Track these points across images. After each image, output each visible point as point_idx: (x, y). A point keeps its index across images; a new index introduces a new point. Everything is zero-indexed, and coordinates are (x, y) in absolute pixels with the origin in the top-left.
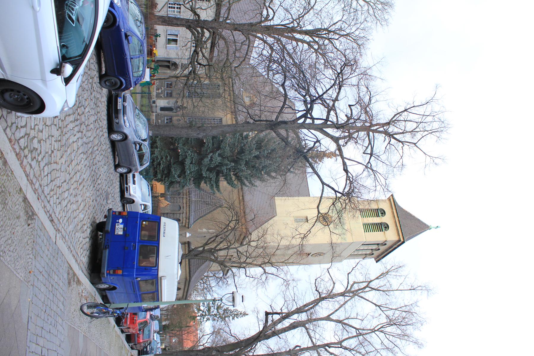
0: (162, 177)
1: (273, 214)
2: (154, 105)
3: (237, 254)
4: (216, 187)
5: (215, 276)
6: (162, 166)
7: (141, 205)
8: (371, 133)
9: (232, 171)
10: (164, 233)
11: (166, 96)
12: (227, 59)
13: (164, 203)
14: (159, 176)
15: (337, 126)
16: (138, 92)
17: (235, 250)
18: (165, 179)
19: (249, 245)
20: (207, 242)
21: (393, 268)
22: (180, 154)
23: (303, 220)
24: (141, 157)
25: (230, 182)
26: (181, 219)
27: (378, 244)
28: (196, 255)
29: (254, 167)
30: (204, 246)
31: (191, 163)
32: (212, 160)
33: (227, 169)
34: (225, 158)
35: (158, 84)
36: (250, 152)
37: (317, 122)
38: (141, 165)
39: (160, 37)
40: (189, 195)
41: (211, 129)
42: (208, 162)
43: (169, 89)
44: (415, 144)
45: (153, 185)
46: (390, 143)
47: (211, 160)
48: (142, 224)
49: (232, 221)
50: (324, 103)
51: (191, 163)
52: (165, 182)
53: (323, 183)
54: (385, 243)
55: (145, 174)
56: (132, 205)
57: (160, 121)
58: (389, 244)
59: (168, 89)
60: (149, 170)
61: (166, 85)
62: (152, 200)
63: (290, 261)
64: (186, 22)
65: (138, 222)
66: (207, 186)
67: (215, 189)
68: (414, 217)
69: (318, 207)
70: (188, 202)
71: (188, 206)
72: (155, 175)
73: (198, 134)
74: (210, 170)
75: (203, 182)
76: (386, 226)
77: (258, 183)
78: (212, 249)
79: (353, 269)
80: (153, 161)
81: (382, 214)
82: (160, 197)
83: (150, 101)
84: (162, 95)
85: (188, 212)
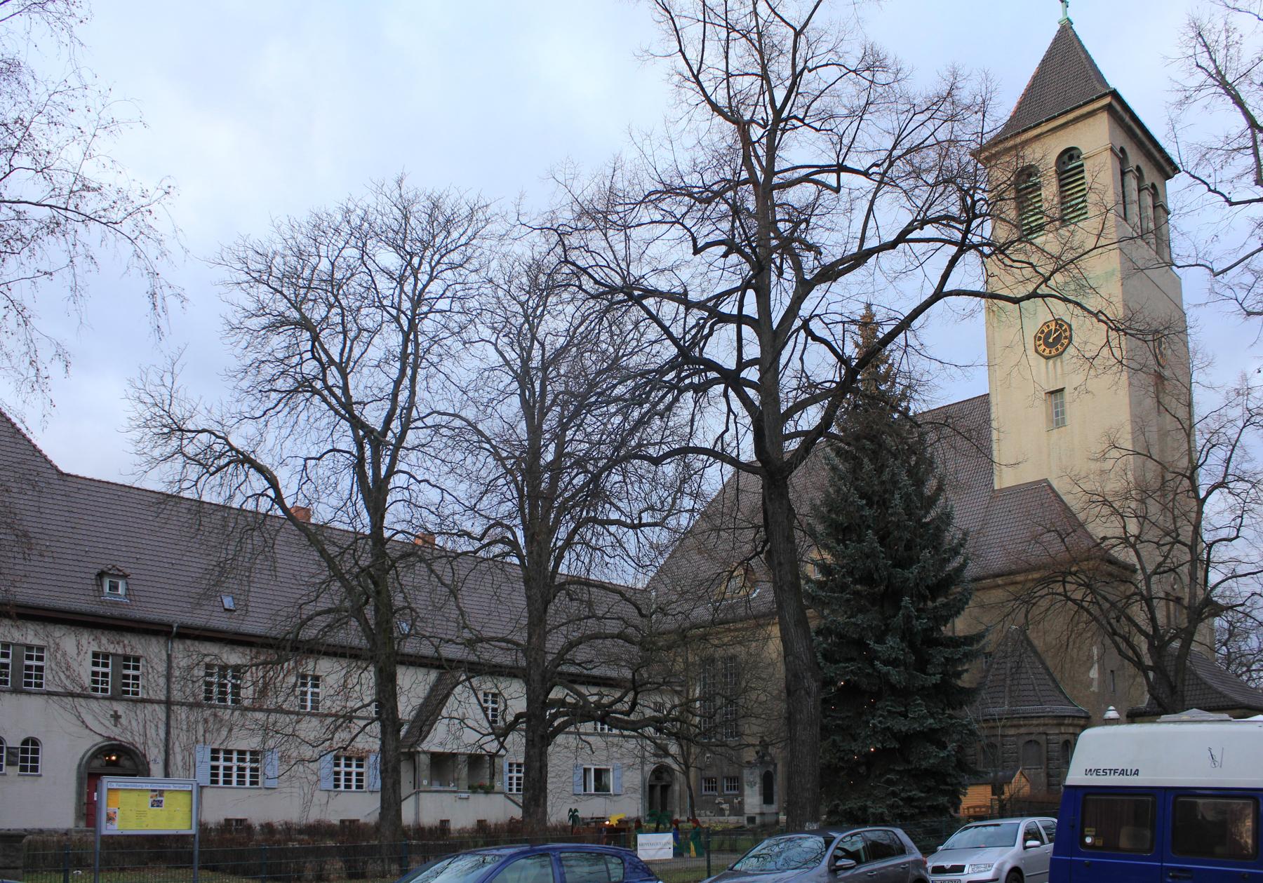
0: (944, 793)
1: (1043, 489)
2: (758, 820)
3: (1165, 572)
4: (971, 644)
5: (1228, 640)
6: (916, 793)
7: (1025, 848)
8: (776, 180)
9: (925, 604)
10: (1123, 772)
11: (736, 792)
12: (619, 636)
13: (1019, 784)
14: (943, 800)
15: (758, 282)
16: (705, 864)
17: (1154, 579)
18: (952, 785)
19: (1137, 537)
20: (1130, 659)
21: (1204, 60)
22: (879, 746)
23: (1056, 404)
24: (877, 851)
25: (956, 609)
26: (1062, 738)
27: (1123, 174)
28: (1173, 689)
29: (909, 547)
30: (1144, 669)
31: (906, 717)
32: (896, 659)
33: (918, 618)
34: (887, 625)
35: (708, 813)
36: (868, 557)
37: (753, 350)
38: (902, 851)
39: (576, 810)
40: (994, 720)
41: (791, 658)
42: (899, 672)
43: (719, 783)
44: (798, 34)
45: (970, 817)
46: (801, 117)
47: (894, 663)
48: (1092, 846)
49: (1066, 596)
50: (701, 337)
51: (906, 717)
52: (960, 783)
53: (939, 295)
54: (1118, 151)
55: (931, 839)
56: (1026, 874)
58: (1122, 141)
59: (719, 788)
60: (925, 826)
61: (711, 793)
62: (1012, 816)
63: (1182, 413)
64: (534, 746)
65: (1087, 860)
66: (966, 671)
67: (975, 647)
68: (1035, 78)
69: (1016, 301)
70: (1015, 722)
71: (1026, 722)
72: (941, 810)
73: (808, 693)
74: (922, 665)
75: (959, 683)
76: (1066, 157)
77: (952, 535)
78: (1151, 645)
79: (1215, 191)
80: (901, 819)
82: (1003, 797)
83: (748, 830)
84: (735, 801)
85: (1042, 721)
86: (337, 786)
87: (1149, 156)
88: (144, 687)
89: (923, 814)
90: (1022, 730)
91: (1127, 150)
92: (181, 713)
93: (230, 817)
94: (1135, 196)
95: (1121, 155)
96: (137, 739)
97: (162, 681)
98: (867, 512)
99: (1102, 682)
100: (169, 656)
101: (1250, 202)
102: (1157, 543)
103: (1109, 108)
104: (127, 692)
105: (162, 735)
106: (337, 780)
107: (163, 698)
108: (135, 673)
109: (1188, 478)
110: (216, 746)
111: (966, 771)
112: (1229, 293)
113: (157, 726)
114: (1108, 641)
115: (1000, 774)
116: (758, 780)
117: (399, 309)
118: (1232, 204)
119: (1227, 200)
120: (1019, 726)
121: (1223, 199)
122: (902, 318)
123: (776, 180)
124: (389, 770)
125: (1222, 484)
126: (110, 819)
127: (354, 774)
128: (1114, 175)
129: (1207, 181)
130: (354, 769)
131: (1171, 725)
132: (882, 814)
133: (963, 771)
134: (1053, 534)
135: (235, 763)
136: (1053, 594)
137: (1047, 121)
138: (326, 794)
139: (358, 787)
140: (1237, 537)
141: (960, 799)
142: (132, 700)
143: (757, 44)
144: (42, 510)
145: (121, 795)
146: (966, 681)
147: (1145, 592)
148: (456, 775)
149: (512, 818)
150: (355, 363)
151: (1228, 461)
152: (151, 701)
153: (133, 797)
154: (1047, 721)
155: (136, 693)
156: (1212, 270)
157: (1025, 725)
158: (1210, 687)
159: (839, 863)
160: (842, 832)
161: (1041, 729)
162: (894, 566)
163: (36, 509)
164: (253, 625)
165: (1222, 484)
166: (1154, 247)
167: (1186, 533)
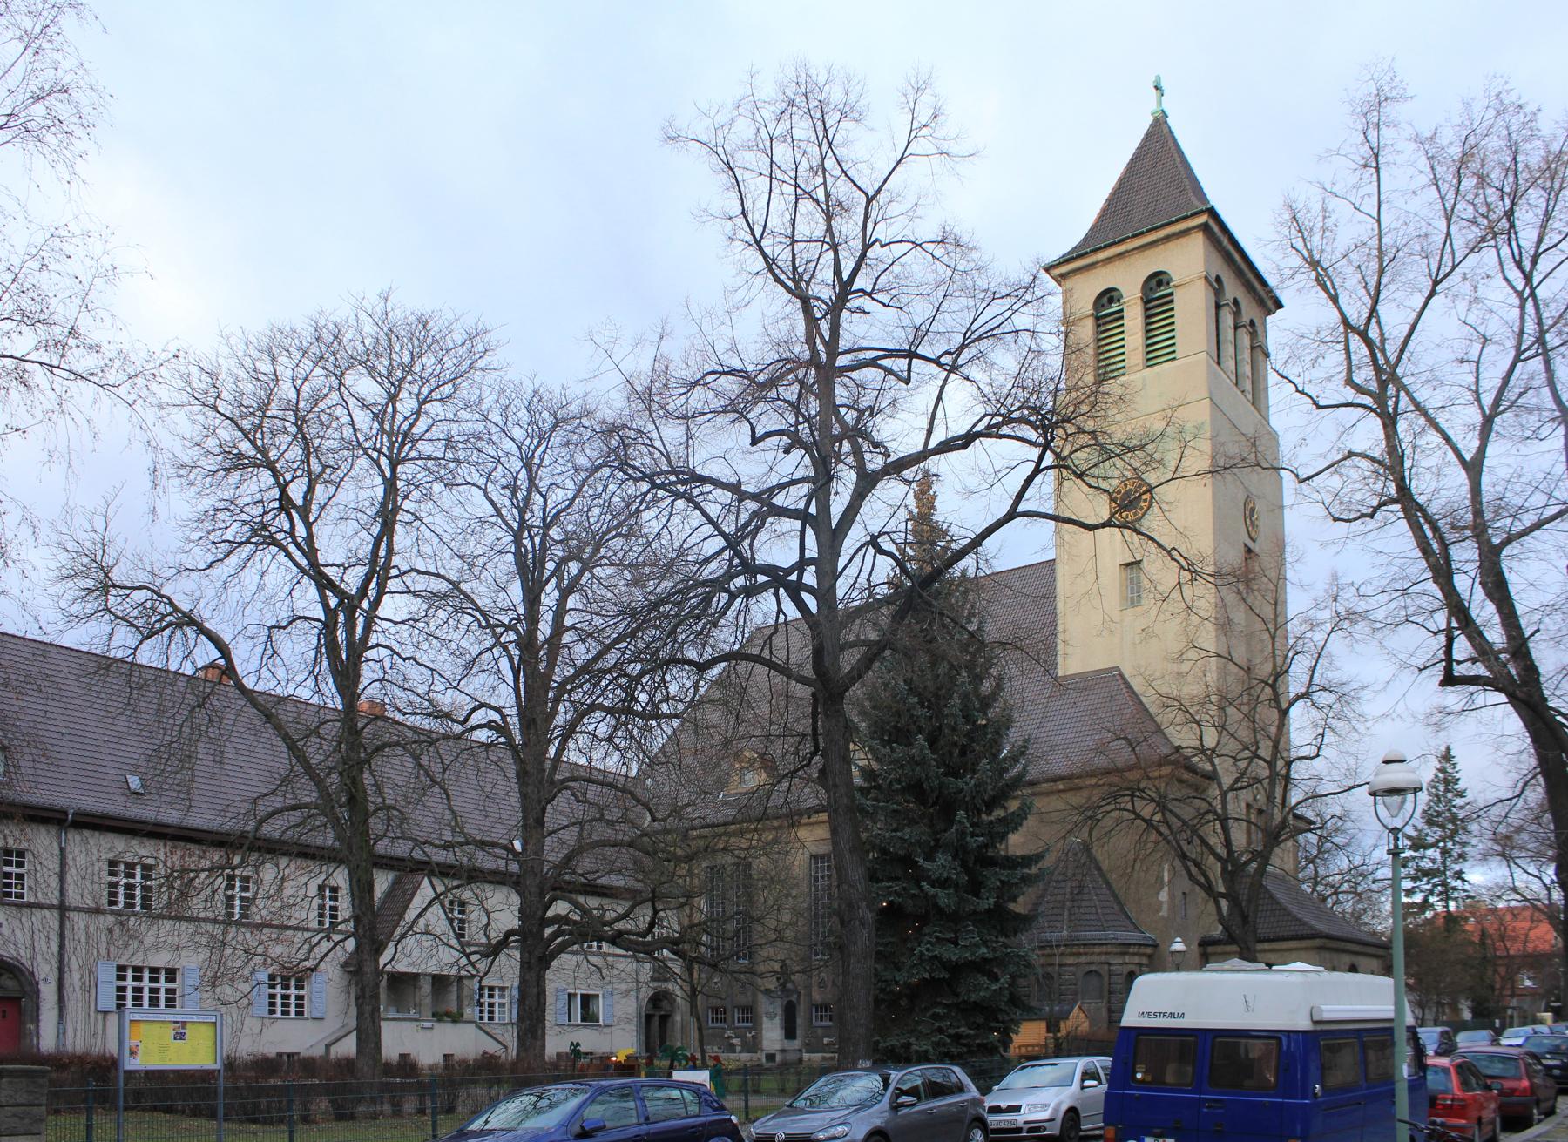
1: (1114, 677)
2: (778, 1058)
3: (1242, 788)
7: (1083, 1088)
10: (1171, 1015)
11: (750, 1025)
13: (1077, 1021)
15: (822, 482)
16: (742, 1104)
17: (1230, 795)
18: (1003, 1022)
19: (1213, 751)
20: (1200, 885)
21: (1299, 244)
25: (1013, 822)
26: (1126, 970)
27: (1218, 307)
28: (1245, 918)
31: (956, 944)
34: (937, 840)
35: (716, 1048)
37: (812, 551)
38: (961, 1089)
39: (578, 1044)
43: (729, 1014)
44: (870, 200)
47: (943, 883)
48: (1142, 1081)
49: (1134, 812)
50: (750, 530)
51: (956, 944)
53: (1011, 515)
55: (988, 1078)
56: (1082, 1115)
57: (826, 1040)
58: (1219, 268)
59: (729, 1019)
61: (718, 1025)
63: (1268, 612)
67: (1034, 870)
68: (1122, 181)
70: (1075, 950)
71: (1087, 950)
72: (990, 1050)
73: (863, 924)
74: (975, 887)
78: (1224, 870)
79: (1302, 393)
81: (1111, 301)
85: (1104, 949)
86: (272, 1012)
87: (1249, 287)
88: (30, 888)
89: (970, 1052)
90: (1083, 959)
91: (1224, 279)
92: (78, 920)
93: (560, 1051)
94: (1231, 333)
95: (1216, 285)
96: (22, 953)
97: (54, 881)
98: (918, 712)
99: (1172, 908)
100: (62, 850)
101: (1337, 406)
102: (1234, 758)
103: (1205, 228)
104: (9, 895)
105: (55, 948)
106: (272, 1004)
107: (56, 902)
108: (19, 870)
109: (1271, 686)
110: (122, 962)
111: (1021, 1007)
112: (1315, 496)
113: (47, 937)
114: (1177, 863)
115: (1057, 1008)
116: (779, 1011)
117: (380, 452)
118: (1319, 407)
119: (1315, 403)
120: (1079, 954)
121: (1310, 401)
122: (973, 536)
123: (842, 361)
124: (367, 995)
125: (1306, 695)
126: (133, 1053)
127: (279, 996)
128: (1207, 309)
129: (1296, 380)
130: (293, 992)
131: (1214, 974)
132: (926, 1052)
133: (1016, 1006)
134: (1121, 742)
135: (146, 984)
136: (1120, 809)
137: (1133, 236)
138: (259, 1022)
139: (298, 1013)
140: (1318, 756)
141: (1011, 1038)
142: (16, 905)
143: (824, 207)
144: (49, 715)
145: (143, 1027)
146: (1019, 907)
147: (1219, 811)
148: (417, 1000)
149: (485, 1053)
150: (322, 508)
151: (1313, 669)
152: (40, 906)
153: (156, 1028)
154: (1110, 949)
155: (22, 896)
156: (1297, 476)
157: (1086, 954)
158: (1289, 914)
159: (900, 1100)
160: (900, 1070)
161: (1103, 958)
162: (946, 774)
163: (42, 714)
164: (200, 819)
165: (1306, 695)
166: (1250, 397)
167: (1265, 751)
